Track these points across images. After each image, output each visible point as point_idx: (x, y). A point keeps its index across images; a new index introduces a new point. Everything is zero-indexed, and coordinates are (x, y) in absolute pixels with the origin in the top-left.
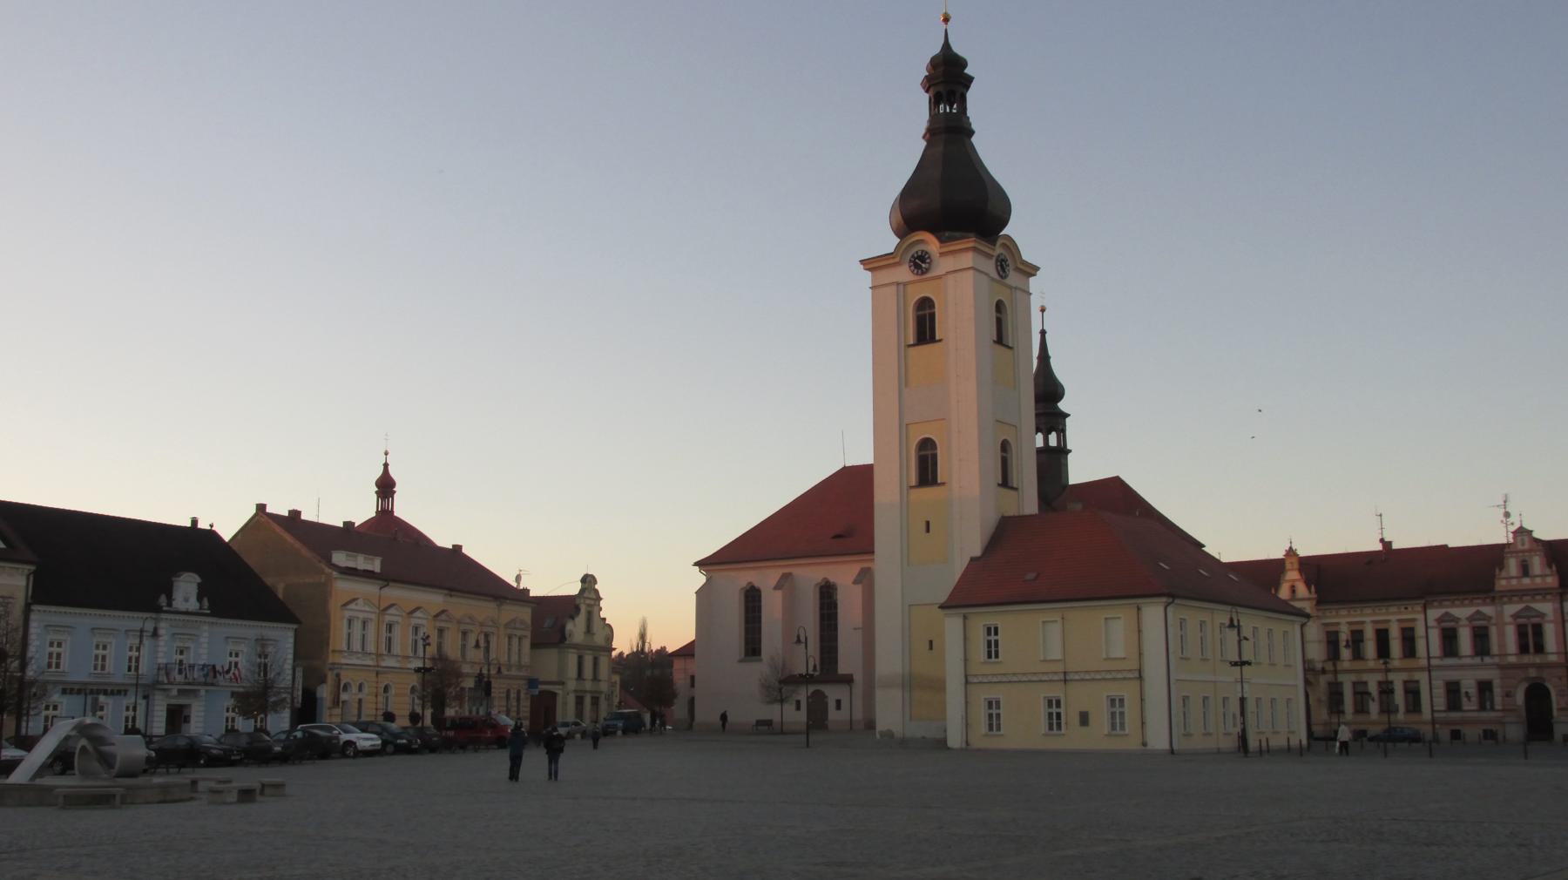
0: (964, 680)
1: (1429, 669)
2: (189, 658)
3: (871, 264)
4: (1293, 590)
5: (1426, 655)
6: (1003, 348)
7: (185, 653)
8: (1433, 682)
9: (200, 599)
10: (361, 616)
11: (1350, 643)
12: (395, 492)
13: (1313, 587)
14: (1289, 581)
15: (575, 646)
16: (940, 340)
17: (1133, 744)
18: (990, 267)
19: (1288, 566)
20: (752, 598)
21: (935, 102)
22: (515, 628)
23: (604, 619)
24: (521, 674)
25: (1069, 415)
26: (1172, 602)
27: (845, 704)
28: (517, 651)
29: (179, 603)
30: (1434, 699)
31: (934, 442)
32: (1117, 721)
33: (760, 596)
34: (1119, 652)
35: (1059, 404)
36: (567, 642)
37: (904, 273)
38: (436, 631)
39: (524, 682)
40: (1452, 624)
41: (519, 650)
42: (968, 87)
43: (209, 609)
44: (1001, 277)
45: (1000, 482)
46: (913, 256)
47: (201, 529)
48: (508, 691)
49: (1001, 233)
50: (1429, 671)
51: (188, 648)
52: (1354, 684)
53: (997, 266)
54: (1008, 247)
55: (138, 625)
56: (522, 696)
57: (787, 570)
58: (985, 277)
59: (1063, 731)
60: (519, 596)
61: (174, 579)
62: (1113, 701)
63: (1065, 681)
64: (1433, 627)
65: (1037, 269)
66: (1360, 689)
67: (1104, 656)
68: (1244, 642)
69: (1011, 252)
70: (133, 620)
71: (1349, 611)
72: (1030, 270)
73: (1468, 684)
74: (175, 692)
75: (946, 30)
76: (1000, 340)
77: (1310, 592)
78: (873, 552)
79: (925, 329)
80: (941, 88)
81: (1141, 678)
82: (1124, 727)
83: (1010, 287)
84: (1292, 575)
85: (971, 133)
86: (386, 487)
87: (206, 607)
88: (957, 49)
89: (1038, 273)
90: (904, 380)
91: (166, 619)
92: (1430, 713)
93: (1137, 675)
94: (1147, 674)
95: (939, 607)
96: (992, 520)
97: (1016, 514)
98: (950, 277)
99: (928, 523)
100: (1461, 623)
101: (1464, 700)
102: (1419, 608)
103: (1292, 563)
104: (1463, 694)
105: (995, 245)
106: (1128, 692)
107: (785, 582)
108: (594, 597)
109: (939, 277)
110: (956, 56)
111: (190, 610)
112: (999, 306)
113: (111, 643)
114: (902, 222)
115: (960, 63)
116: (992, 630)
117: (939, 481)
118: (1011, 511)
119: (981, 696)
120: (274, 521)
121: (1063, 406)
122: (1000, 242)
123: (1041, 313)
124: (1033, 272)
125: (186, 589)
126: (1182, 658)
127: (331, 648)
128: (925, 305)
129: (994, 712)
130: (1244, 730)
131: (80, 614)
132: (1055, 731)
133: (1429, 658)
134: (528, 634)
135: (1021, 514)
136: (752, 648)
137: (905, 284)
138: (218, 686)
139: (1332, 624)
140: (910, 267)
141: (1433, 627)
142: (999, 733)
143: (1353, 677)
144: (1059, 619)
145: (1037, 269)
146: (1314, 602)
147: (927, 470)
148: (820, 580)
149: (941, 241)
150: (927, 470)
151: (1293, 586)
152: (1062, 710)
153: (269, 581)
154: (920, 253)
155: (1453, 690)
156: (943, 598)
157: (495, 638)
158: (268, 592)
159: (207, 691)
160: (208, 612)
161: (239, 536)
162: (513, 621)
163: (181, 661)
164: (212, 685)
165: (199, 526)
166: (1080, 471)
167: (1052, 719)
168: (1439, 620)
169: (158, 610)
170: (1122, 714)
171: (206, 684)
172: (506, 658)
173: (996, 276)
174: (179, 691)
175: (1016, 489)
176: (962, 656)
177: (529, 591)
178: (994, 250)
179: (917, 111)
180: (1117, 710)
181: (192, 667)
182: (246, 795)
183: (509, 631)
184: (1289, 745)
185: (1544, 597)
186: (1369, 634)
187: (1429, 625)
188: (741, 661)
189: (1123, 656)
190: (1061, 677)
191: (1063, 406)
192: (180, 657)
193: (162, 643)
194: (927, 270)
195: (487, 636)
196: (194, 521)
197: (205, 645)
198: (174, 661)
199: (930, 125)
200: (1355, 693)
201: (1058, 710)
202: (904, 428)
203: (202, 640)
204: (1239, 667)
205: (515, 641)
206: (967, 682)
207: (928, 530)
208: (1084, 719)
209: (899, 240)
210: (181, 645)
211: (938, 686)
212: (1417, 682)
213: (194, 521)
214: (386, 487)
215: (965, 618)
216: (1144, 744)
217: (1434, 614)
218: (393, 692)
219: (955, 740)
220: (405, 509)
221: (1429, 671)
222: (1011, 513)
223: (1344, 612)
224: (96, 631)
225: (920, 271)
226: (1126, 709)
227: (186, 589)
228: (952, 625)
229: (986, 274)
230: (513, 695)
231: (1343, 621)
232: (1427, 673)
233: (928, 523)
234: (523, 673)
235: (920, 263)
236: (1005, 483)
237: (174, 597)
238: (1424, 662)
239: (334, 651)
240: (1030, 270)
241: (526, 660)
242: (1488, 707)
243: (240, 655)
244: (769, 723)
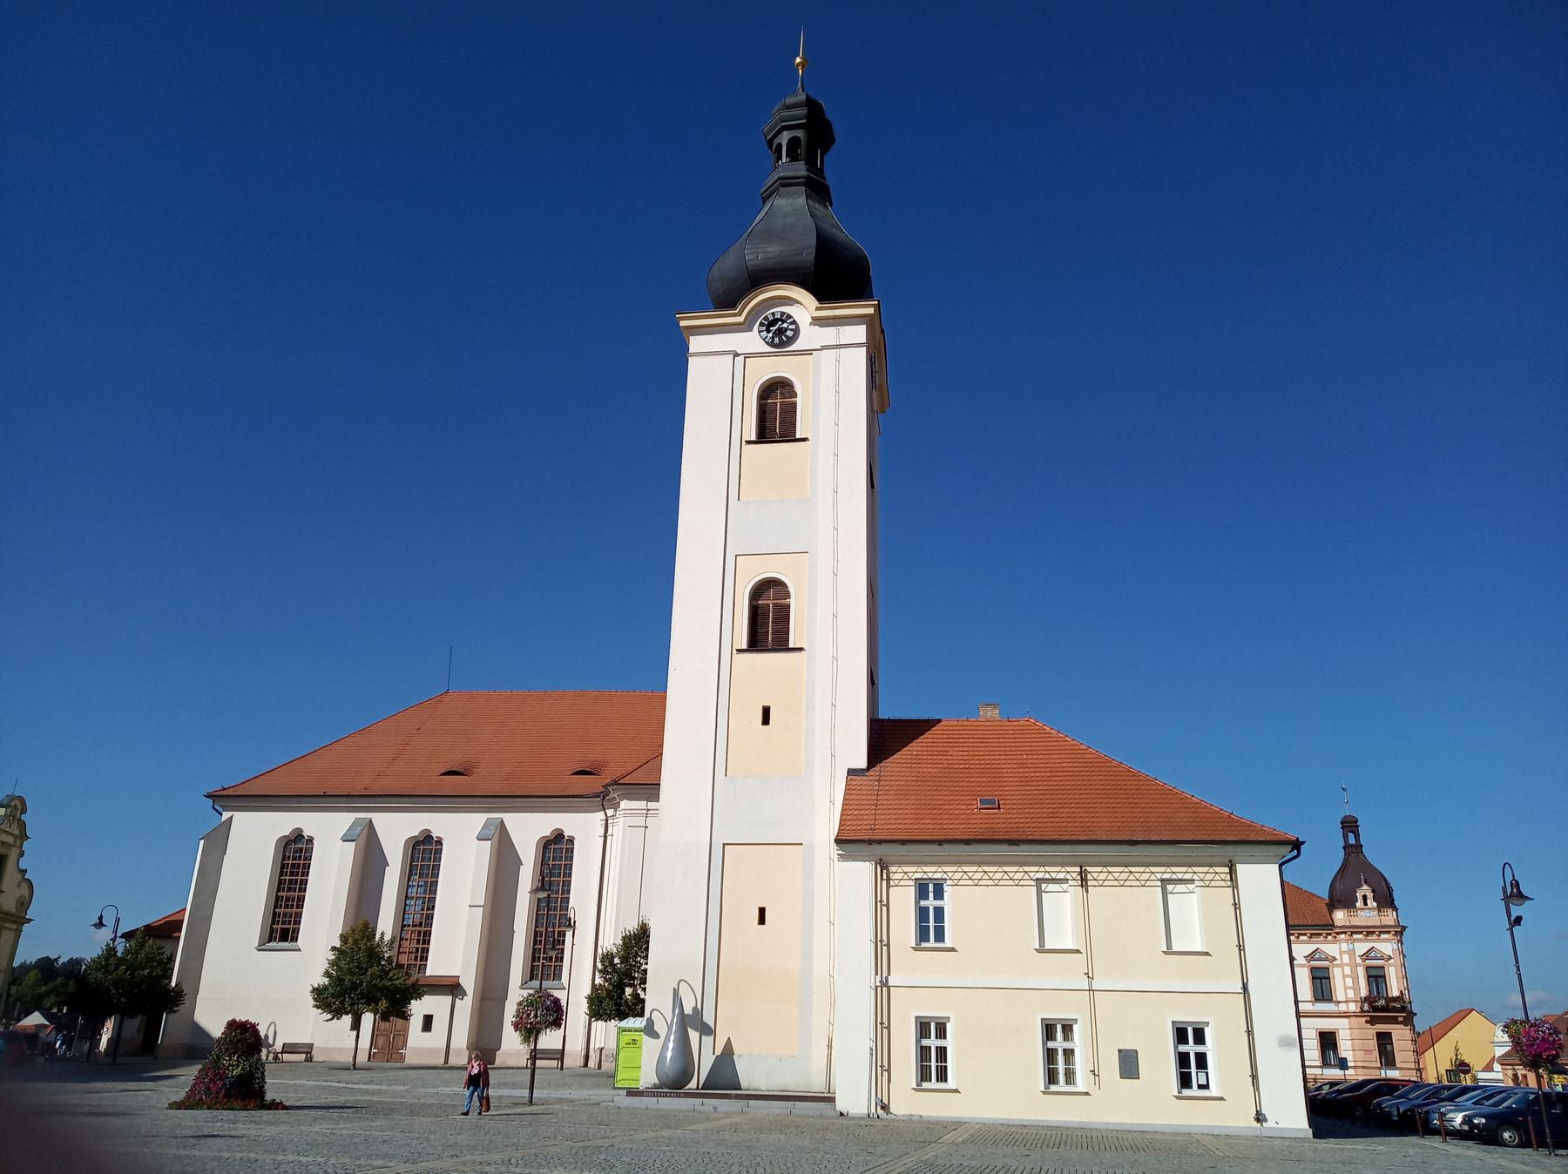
23: (25, 871)
27: (440, 1024)
32: (1190, 1068)
46: (766, 318)
108: (17, 832)
117: (791, 646)
130: (285, 1108)
137: (747, 356)
140: (760, 332)
168: (1311, 957)
180: (932, 1042)
185: (1298, 937)
201: (941, 1043)
208: (1129, 1064)
216: (1260, 1118)
239: (1260, 1118)
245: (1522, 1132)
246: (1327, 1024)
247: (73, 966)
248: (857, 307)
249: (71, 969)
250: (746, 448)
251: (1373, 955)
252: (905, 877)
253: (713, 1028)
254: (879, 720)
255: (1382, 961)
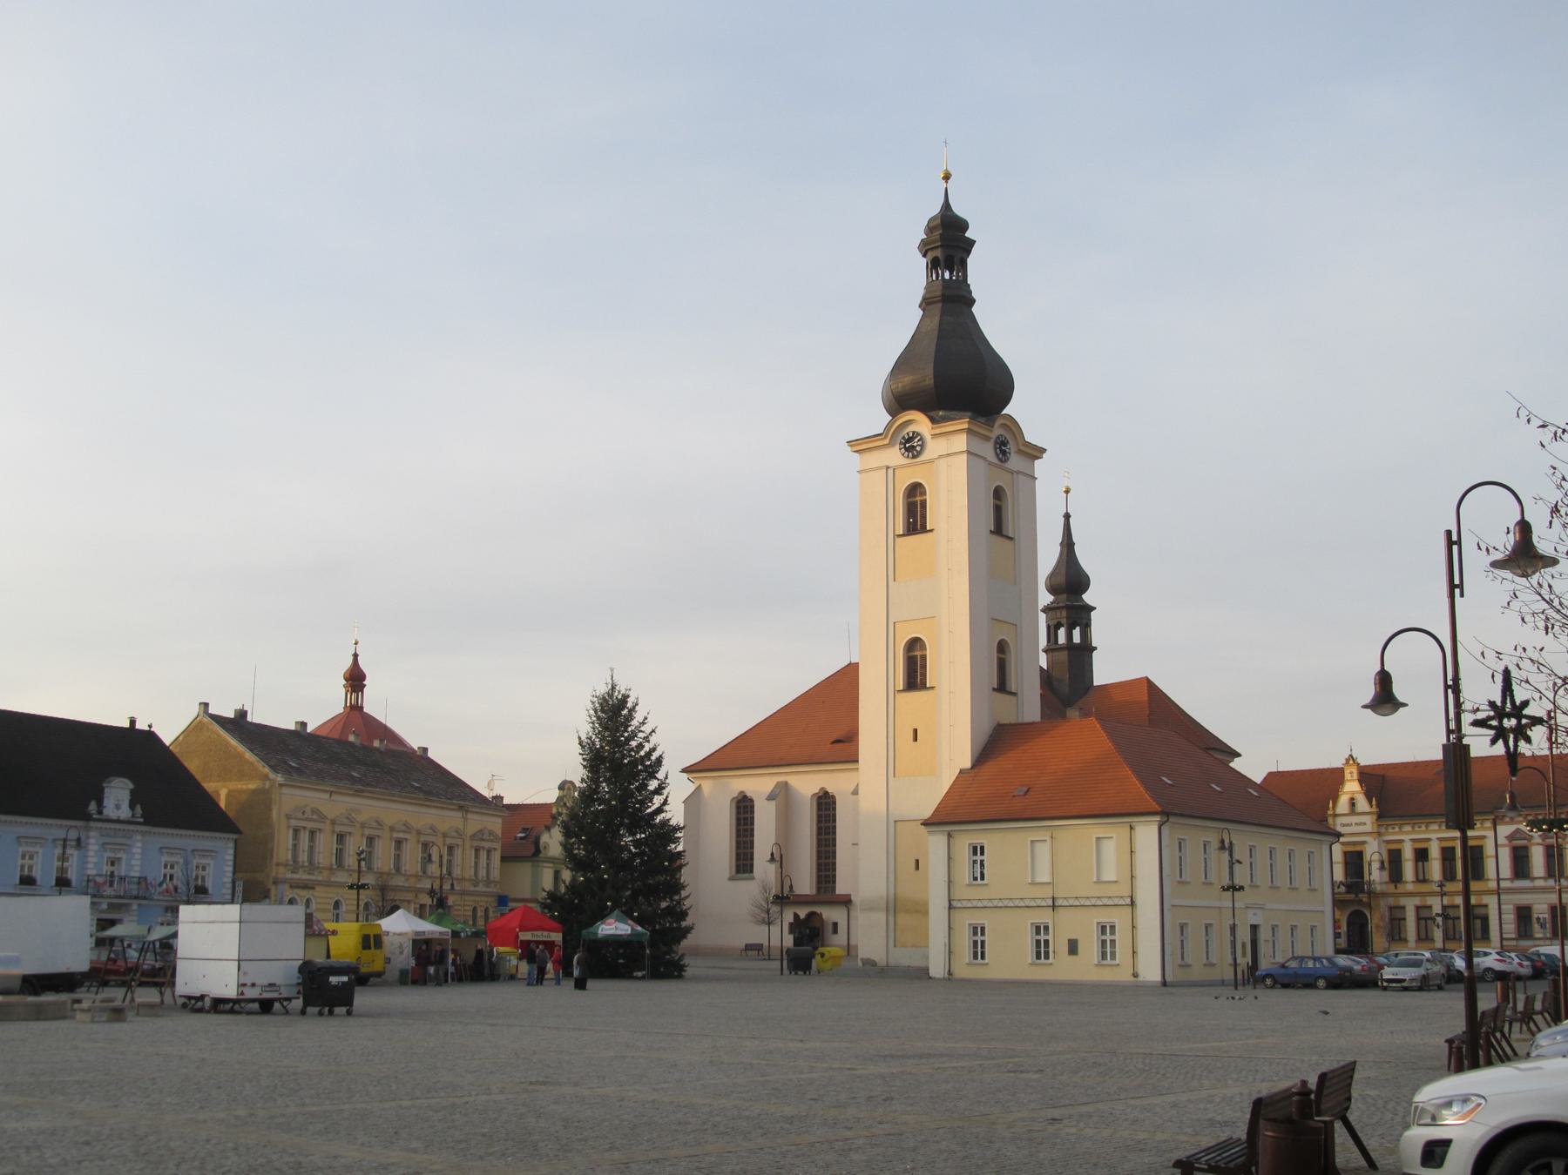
0: (947, 905)
1: (1498, 892)
2: (122, 870)
3: (861, 445)
4: (1352, 803)
5: (1495, 877)
6: (1003, 540)
7: (116, 865)
8: (1503, 907)
9: (132, 806)
10: (310, 825)
11: (1386, 864)
12: (365, 686)
13: (1374, 799)
14: (1347, 793)
15: (552, 860)
16: (931, 531)
17: (1124, 975)
18: (988, 450)
19: (1347, 776)
20: (744, 808)
21: (934, 265)
22: (483, 840)
24: (488, 890)
25: (1095, 608)
26: (1167, 821)
28: (485, 865)
29: (110, 811)
30: (1503, 926)
31: (923, 641)
33: (753, 807)
34: (1110, 874)
35: (1084, 596)
36: (541, 855)
37: (894, 456)
38: (420, 846)
39: (493, 899)
40: (1523, 842)
41: (488, 864)
42: (969, 252)
43: (142, 816)
44: (1001, 460)
45: (996, 687)
46: (904, 438)
47: (138, 730)
48: (475, 910)
49: (1003, 413)
50: (1499, 894)
51: (119, 859)
52: (1418, 908)
53: (996, 449)
54: (1008, 426)
55: (61, 834)
56: (491, 914)
57: (782, 779)
58: (983, 461)
59: (1051, 960)
60: (495, 804)
61: (105, 785)
62: (1103, 928)
63: (1054, 907)
64: (1503, 846)
65: (1044, 450)
66: (1424, 914)
67: (1095, 880)
68: (1237, 866)
69: (1013, 433)
70: (55, 829)
71: (1413, 828)
72: (1036, 452)
73: (1541, 909)
74: (104, 906)
75: (946, 189)
76: (998, 530)
77: (1371, 806)
78: (857, 761)
79: (915, 518)
80: (938, 253)
81: (1133, 904)
82: (1115, 957)
83: (1012, 472)
84: (1352, 787)
85: (973, 301)
86: (355, 680)
87: (139, 816)
88: (959, 209)
89: (1044, 455)
90: (892, 573)
91: (96, 828)
92: (1499, 939)
93: (1128, 901)
94: (1140, 899)
95: (922, 824)
96: (987, 728)
97: (1013, 722)
98: (942, 461)
99: (915, 731)
100: (1534, 841)
101: (1536, 926)
102: (1488, 824)
103: (1351, 773)
104: (1534, 921)
105: (993, 427)
106: (1120, 919)
107: (782, 794)
109: (931, 461)
110: (957, 217)
111: (121, 818)
112: (998, 493)
113: (37, 853)
114: (894, 400)
115: (962, 225)
116: (977, 850)
117: (928, 686)
118: (1008, 719)
119: (965, 920)
120: (218, 723)
121: (1088, 597)
122: (999, 422)
123: (1065, 495)
124: (1039, 455)
125: (117, 796)
126: (1179, 882)
127: (275, 860)
128: (915, 490)
129: (1108, 937)
131: (11, 822)
132: (1043, 960)
133: (1498, 880)
134: (498, 846)
135: (1020, 721)
136: (743, 863)
138: (151, 899)
139: (1354, 843)
140: (900, 449)
141: (1503, 846)
142: (1113, 962)
143: (1417, 901)
144: (1048, 838)
145: (1044, 450)
146: (1375, 817)
147: (915, 676)
148: (736, 795)
149: (933, 420)
150: (915, 676)
151: (1352, 799)
152: (1050, 937)
153: (209, 786)
154: (911, 435)
155: (1524, 914)
156: (927, 813)
157: (460, 850)
158: (209, 801)
159: (139, 905)
160: (142, 820)
161: (181, 738)
162: (481, 831)
163: (112, 873)
164: (145, 898)
165: (137, 727)
166: (1105, 671)
167: (1040, 948)
168: (1511, 838)
169: (87, 817)
170: (1113, 942)
171: (136, 898)
172: (472, 873)
173: (994, 460)
174: (110, 905)
175: (1014, 694)
176: (946, 879)
177: (502, 798)
178: (992, 431)
179: (914, 276)
180: (1042, 937)
181: (122, 879)
182: (118, 1014)
183: (476, 843)
184: (887, 962)
186: (1408, 854)
187: (1499, 843)
188: (731, 879)
189: (1115, 879)
190: (1050, 902)
191: (1088, 597)
192: (111, 868)
193: (91, 853)
194: (919, 453)
195: (451, 849)
196: (133, 722)
197: (138, 856)
198: (104, 873)
199: (926, 293)
200: (1419, 919)
202: (891, 627)
203: (135, 850)
204: (355, 891)
205: (483, 855)
206: (950, 907)
207: (915, 739)
208: (1073, 948)
209: (891, 418)
210: (112, 855)
211: (921, 910)
212: (1486, 906)
213: (133, 722)
214: (355, 680)
215: (949, 836)
216: (1135, 975)
217: (1505, 830)
218: (344, 909)
219: (937, 969)
220: (374, 703)
221: (1499, 894)
222: (1006, 721)
223: (1407, 828)
224: (22, 840)
225: (910, 454)
226: (1117, 937)
227: (117, 796)
228: (936, 843)
229: (984, 459)
230: (480, 913)
231: (1406, 837)
232: (1496, 896)
233: (915, 731)
234: (493, 889)
235: (912, 446)
236: (1002, 687)
237: (105, 804)
238: (1493, 885)
240: (1036, 452)
241: (496, 874)
242: (1397, 937)
243: (176, 867)
244: (758, 948)
245: (535, 966)
246: (1524, 899)
247: (303, 1012)
248: (956, 424)
249: (309, 1009)
250: (899, 540)
251: (1518, 836)
252: (964, 841)
253: (1336, 909)
254: (345, 1005)
255: (1526, 841)
